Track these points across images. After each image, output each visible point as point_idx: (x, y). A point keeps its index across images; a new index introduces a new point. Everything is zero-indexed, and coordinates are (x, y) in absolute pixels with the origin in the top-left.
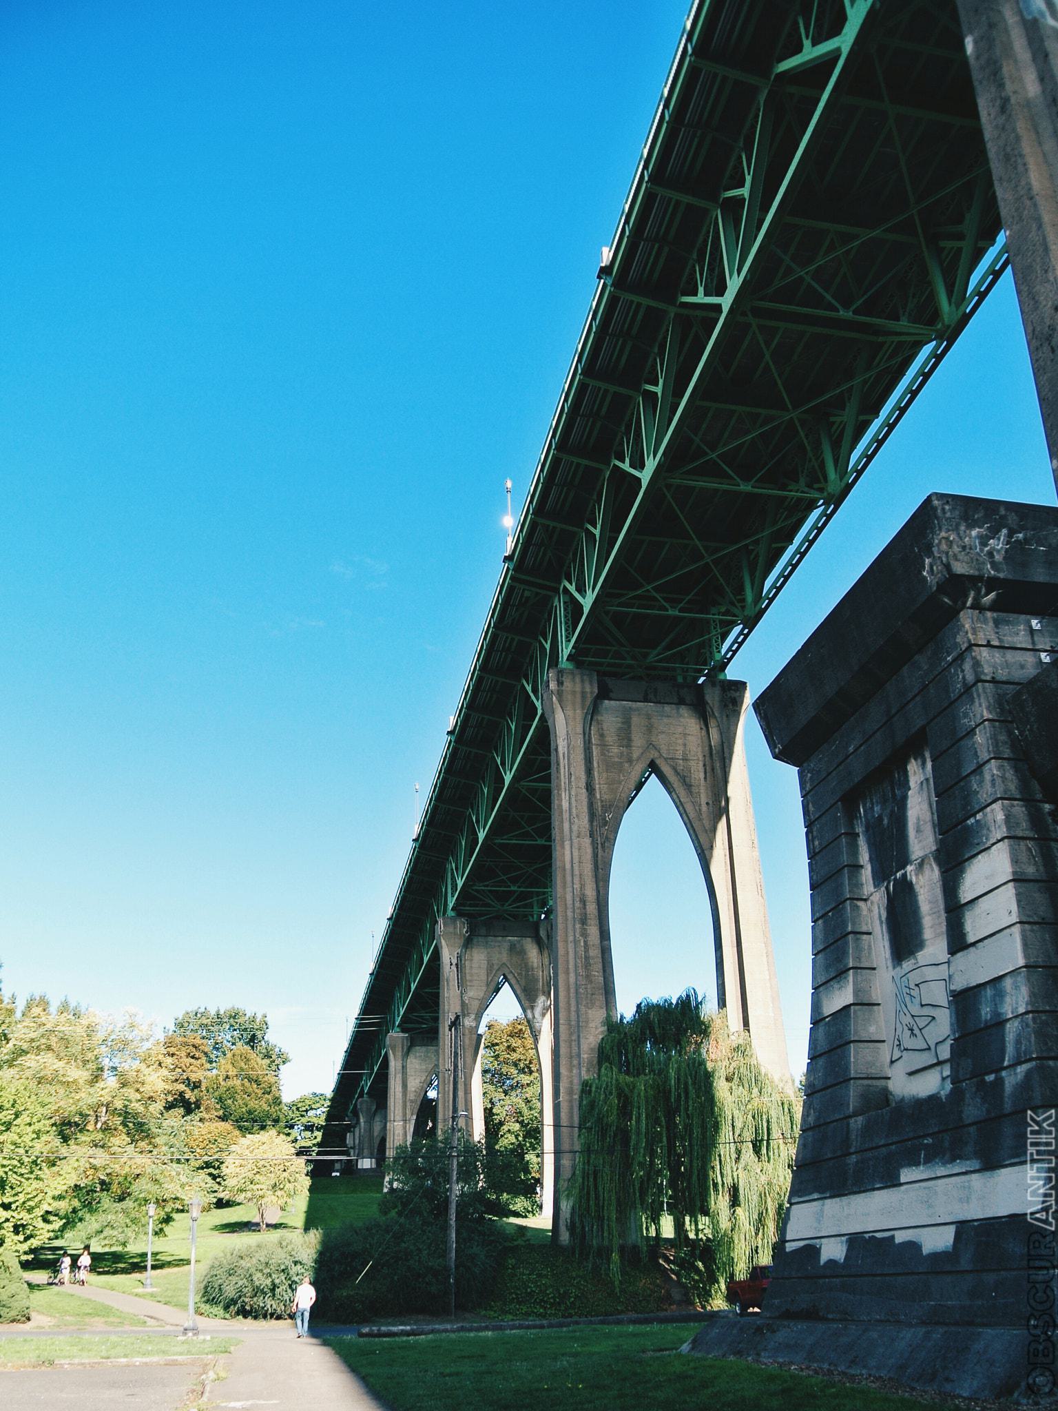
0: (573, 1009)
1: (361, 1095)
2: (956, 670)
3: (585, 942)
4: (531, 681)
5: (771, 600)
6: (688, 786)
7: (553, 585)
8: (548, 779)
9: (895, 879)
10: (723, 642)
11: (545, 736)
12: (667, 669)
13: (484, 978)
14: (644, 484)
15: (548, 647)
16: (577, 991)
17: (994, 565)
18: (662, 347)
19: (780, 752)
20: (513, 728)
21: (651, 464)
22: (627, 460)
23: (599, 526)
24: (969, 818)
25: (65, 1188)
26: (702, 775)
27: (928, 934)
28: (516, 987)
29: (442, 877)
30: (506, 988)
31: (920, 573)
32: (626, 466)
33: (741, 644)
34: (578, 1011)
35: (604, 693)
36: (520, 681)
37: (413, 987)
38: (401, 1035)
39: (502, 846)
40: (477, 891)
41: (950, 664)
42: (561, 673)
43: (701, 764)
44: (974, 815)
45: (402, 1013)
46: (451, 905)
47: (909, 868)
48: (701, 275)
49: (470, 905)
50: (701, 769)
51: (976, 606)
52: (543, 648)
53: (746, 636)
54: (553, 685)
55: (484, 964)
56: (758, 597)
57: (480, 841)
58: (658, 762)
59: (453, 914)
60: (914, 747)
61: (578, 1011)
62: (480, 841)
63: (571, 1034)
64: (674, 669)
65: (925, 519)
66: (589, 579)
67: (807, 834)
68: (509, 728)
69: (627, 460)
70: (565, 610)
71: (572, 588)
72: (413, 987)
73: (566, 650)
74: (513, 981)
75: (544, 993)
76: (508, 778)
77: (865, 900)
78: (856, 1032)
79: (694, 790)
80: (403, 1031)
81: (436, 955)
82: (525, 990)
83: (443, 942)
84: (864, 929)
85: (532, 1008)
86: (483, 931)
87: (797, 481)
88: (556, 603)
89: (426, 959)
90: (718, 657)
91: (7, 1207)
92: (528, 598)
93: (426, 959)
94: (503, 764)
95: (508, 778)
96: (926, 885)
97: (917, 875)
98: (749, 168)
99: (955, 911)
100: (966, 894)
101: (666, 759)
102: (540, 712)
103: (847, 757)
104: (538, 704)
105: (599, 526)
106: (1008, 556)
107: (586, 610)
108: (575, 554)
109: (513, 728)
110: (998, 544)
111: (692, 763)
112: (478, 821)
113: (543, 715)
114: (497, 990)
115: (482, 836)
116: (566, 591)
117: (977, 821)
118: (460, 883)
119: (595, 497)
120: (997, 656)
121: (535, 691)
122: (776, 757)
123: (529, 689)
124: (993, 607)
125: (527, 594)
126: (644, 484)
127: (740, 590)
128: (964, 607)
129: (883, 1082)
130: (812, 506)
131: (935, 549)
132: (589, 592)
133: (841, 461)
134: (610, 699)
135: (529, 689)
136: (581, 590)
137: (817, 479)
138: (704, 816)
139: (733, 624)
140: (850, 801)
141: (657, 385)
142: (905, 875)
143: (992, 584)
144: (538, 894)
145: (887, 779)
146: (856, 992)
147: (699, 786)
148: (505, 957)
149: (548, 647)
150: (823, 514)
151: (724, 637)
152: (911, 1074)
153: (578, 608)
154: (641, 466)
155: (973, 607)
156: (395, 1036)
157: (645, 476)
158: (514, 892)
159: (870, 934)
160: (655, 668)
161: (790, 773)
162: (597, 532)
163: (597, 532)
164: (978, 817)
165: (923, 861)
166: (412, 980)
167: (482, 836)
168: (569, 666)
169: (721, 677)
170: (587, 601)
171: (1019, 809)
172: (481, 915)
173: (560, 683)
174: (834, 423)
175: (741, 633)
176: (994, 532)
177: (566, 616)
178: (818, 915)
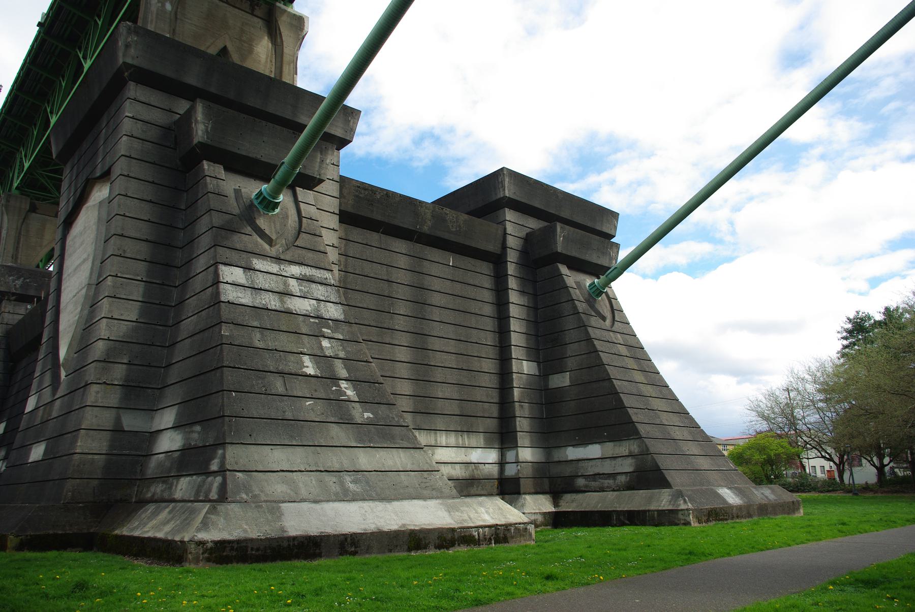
17: (16, 289)
20: (64, 84)
46: (15, 185)
51: (8, 299)
62: (52, 125)
68: (33, 134)
106: (21, 286)
109: (64, 84)
110: (19, 283)
118: (27, 165)
120: (11, 316)
122: (502, 169)
123: (49, 110)
124: (15, 300)
132: (88, 61)
136: (85, 58)
143: (14, 294)
162: (100, 23)
171: (168, 464)
176: (19, 278)
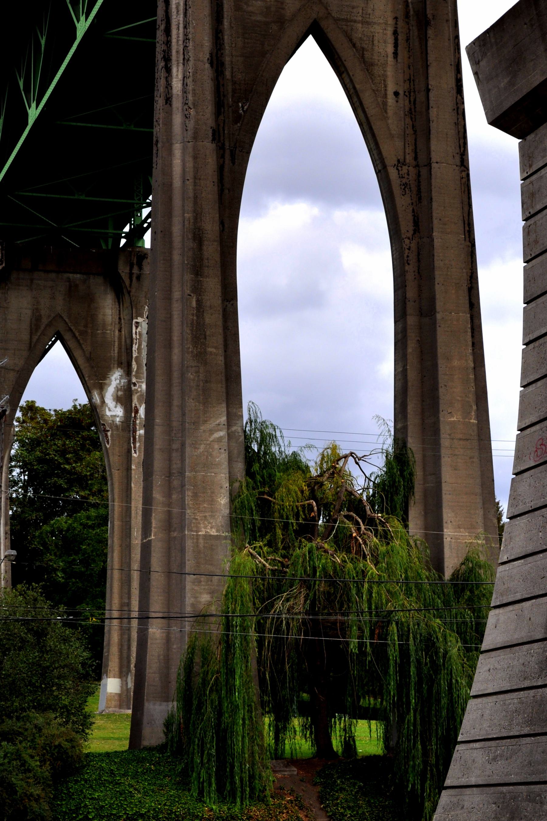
0: (176, 402)
6: (368, 66)
13: (25, 336)
16: (182, 375)
20: (43, 42)
25: (495, 588)
26: (390, 49)
34: (182, 407)
43: (390, 31)
50: (390, 39)
55: (27, 313)
58: (323, 24)
61: (182, 407)
63: (170, 441)
75: (120, 365)
79: (377, 71)
82: (89, 359)
85: (101, 388)
91: (213, 819)
101: (336, 20)
109: (43, 42)
111: (377, 29)
138: (390, 113)
147: (385, 64)
148: (60, 305)
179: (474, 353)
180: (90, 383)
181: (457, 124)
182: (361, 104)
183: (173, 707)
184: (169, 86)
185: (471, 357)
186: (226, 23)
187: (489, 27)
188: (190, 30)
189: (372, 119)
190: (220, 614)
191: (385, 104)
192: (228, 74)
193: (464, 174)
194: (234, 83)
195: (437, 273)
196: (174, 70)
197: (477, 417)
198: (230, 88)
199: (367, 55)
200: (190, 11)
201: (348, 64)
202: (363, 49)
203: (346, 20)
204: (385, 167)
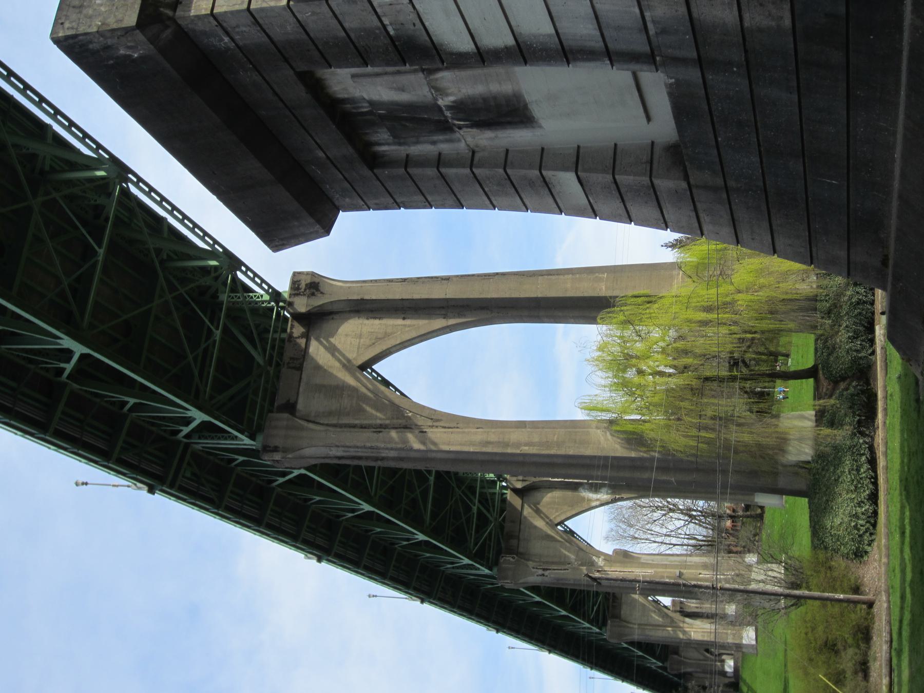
1: (664, 669)
2: (238, 33)
3: (526, 445)
4: (398, 541)
5: (216, 242)
7: (181, 448)
8: (370, 470)
9: (453, 119)
10: (253, 291)
11: (333, 470)
12: (273, 347)
14: (86, 350)
15: (241, 459)
18: (96, 395)
19: (323, 228)
20: (379, 530)
21: (67, 342)
22: (63, 365)
23: (126, 399)
24: (388, 33)
27: (507, 88)
28: (569, 514)
29: (460, 578)
30: (570, 524)
31: (134, 61)
32: (69, 367)
33: (256, 275)
35: (290, 408)
36: (274, 489)
37: (564, 613)
38: (609, 627)
39: (434, 516)
40: (476, 544)
41: (232, 39)
42: (266, 449)
44: (384, 26)
45: (587, 625)
46: (487, 571)
47: (440, 102)
48: (47, 363)
49: (489, 553)
52: (243, 463)
53: (248, 268)
54: (277, 456)
56: (213, 254)
57: (426, 538)
59: (495, 570)
60: (316, 87)
62: (426, 538)
64: (274, 340)
65: (75, 47)
66: (178, 413)
67: (406, 208)
69: (63, 365)
70: (206, 438)
71: (186, 430)
72: (564, 613)
73: (245, 441)
74: (563, 518)
76: (367, 507)
77: (474, 152)
78: (206, 9)
79: (389, 331)
80: (605, 624)
81: (535, 589)
83: (521, 581)
84: (503, 155)
86: (514, 542)
87: (104, 207)
88: (199, 447)
89: (538, 599)
90: (266, 297)
92: (194, 474)
93: (538, 599)
94: (353, 511)
95: (367, 507)
96: (457, 86)
97: (447, 95)
98: (47, 363)
99: (483, 57)
100: (466, 45)
102: (303, 471)
103: (328, 157)
104: (296, 473)
105: (126, 399)
107: (207, 418)
108: (153, 424)
109: (379, 530)
112: (408, 540)
113: (307, 469)
114: (572, 533)
115: (421, 537)
116: (188, 436)
117: (391, 24)
118: (466, 561)
119: (98, 400)
121: (284, 474)
122: (327, 230)
123: (350, 515)
125: (188, 475)
126: (86, 350)
127: (206, 270)
128: (173, 19)
129: (657, 151)
130: (126, 193)
131: (110, 42)
132: (189, 414)
133: (89, 164)
134: (296, 402)
135: (350, 515)
136: (187, 421)
137: (103, 186)
139: (235, 279)
140: (373, 161)
141: (127, 402)
142: (449, 108)
144: (482, 487)
145: (347, 119)
146: (565, 169)
149: (241, 459)
150: (136, 185)
151: (248, 290)
152: (649, 119)
153: (204, 425)
154: (69, 353)
155: (175, 10)
156: (608, 634)
157: (79, 349)
158: (478, 508)
159: (507, 151)
160: (271, 356)
161: (346, 220)
162: (132, 401)
163: (132, 401)
164: (386, 22)
165: (434, 88)
166: (557, 614)
167: (421, 537)
168: (260, 438)
169: (286, 296)
170: (199, 417)
172: (499, 543)
173: (276, 449)
174: (51, 167)
175: (245, 274)
177: (212, 438)
178: (488, 202)
179: (563, 275)
180: (587, 507)
181: (423, 283)
182: (409, 340)
183: (363, 107)
184: (393, 459)
185: (566, 276)
186: (357, 422)
187: (215, 197)
188: (359, 444)
189: (419, 334)
190: (724, 373)
191: (409, 326)
192: (388, 422)
193: (454, 279)
194: (393, 418)
195: (513, 296)
196: (383, 455)
197: (603, 273)
198: (395, 421)
199: (380, 336)
200: (348, 444)
201: (385, 348)
202: (377, 338)
203: (358, 348)
204: (448, 327)
